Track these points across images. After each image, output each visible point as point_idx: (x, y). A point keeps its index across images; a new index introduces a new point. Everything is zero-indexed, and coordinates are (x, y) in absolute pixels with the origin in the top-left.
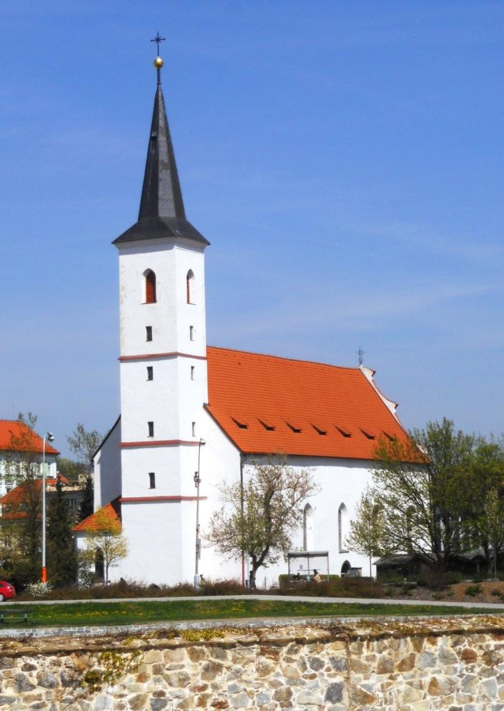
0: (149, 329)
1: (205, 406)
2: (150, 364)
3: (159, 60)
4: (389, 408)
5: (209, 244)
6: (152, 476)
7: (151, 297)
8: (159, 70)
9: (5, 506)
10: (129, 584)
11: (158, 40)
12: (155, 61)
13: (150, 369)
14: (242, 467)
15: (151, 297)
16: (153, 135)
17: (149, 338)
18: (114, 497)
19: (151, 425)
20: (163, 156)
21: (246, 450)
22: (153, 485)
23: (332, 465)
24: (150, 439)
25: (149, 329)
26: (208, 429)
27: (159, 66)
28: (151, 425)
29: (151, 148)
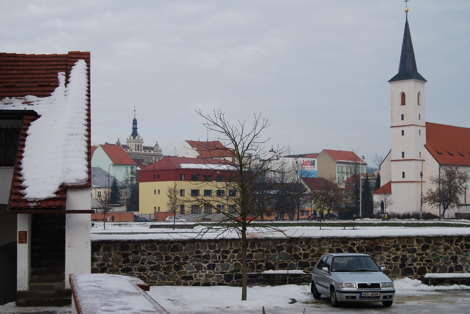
0: (402, 116)
3: (406, 10)
6: (403, 173)
8: (407, 13)
11: (406, 1)
19: (403, 153)
24: (403, 159)
25: (402, 116)
28: (403, 153)
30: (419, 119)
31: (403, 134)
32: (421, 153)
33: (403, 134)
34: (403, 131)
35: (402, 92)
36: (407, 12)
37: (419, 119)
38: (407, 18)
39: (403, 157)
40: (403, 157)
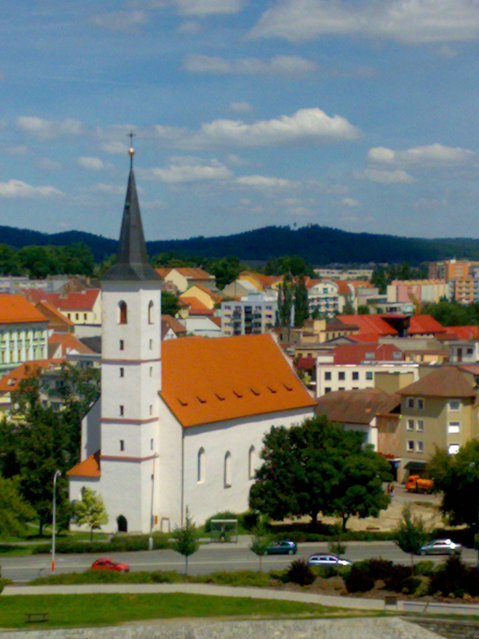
0: (122, 342)
1: (159, 393)
2: (122, 366)
3: (132, 150)
4: (164, 407)
6: (122, 442)
7: (124, 319)
8: (131, 159)
9: (201, 266)
10: (27, 289)
11: (131, 136)
12: (130, 151)
13: (122, 370)
14: (183, 437)
15: (124, 319)
16: (128, 205)
17: (122, 348)
18: (95, 451)
20: (133, 223)
21: (186, 424)
22: (122, 448)
23: (206, 431)
25: (122, 342)
26: (159, 408)
27: (131, 155)
28: (122, 408)
29: (67, 440)
38: (131, 167)
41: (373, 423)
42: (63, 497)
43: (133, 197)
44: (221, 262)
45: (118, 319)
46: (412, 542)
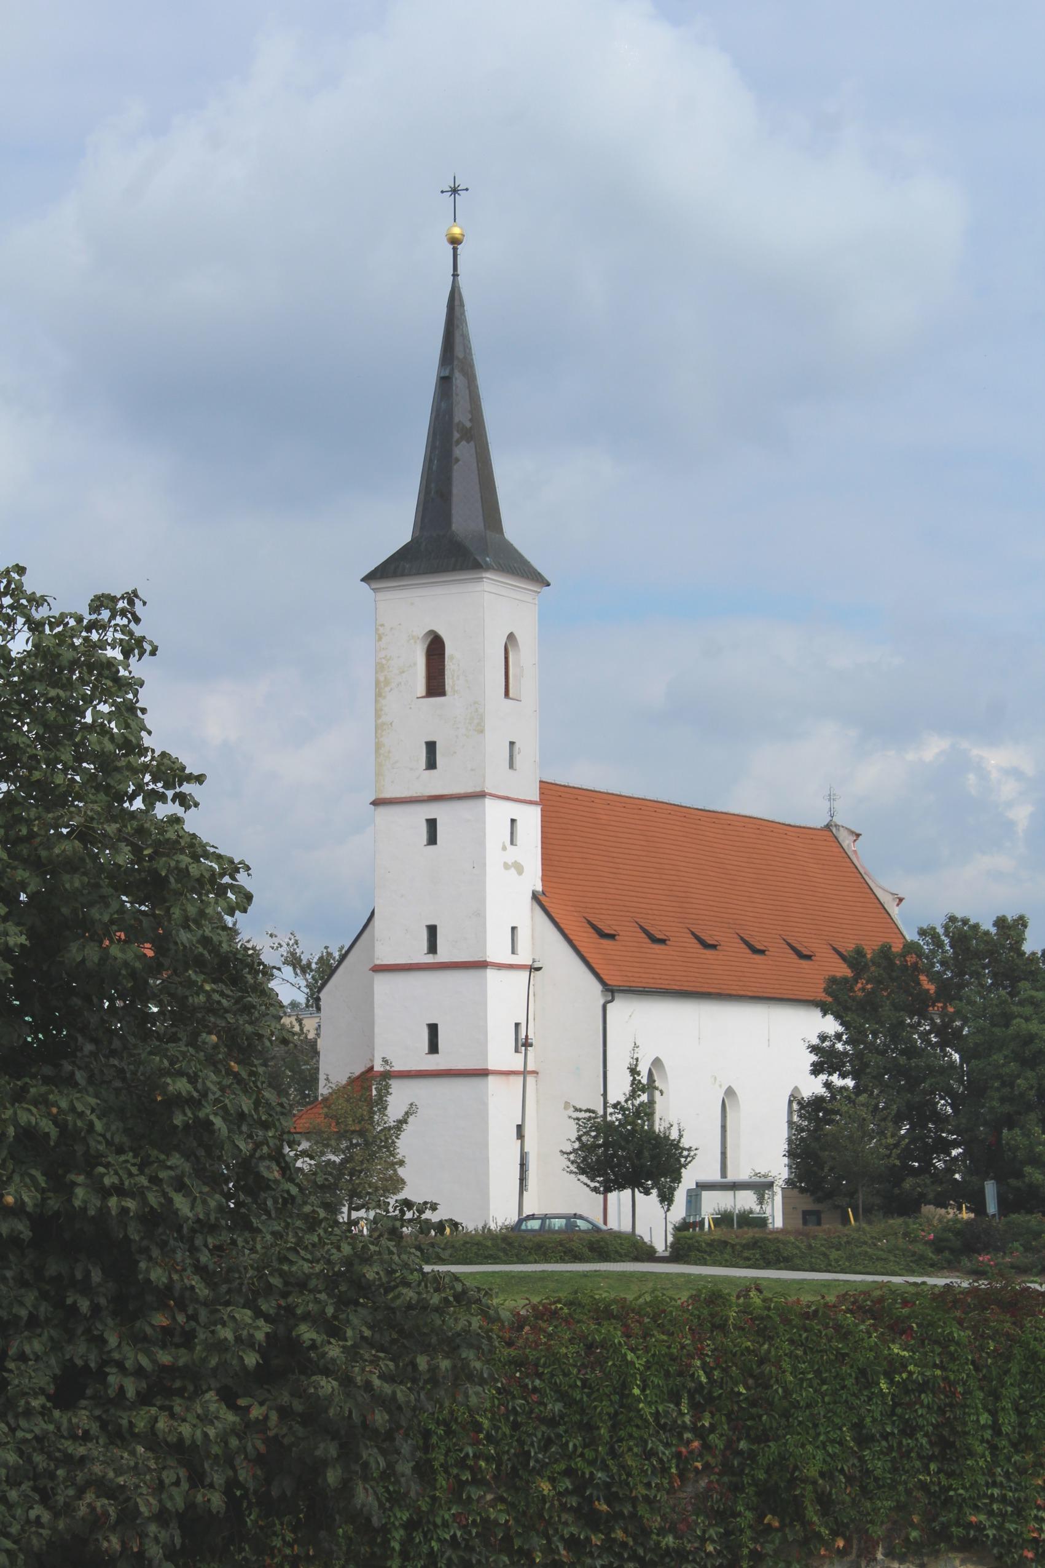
0: (431, 747)
1: (535, 897)
3: (456, 231)
5: (548, 585)
6: (433, 1029)
7: (435, 685)
8: (455, 250)
11: (455, 191)
15: (435, 685)
17: (431, 764)
19: (432, 930)
20: (461, 415)
22: (433, 1048)
24: (430, 959)
25: (431, 747)
28: (432, 930)
30: (511, 766)
31: (432, 840)
32: (519, 824)
33: (432, 840)
34: (432, 824)
35: (432, 632)
36: (455, 242)
37: (511, 766)
38: (455, 275)
39: (432, 948)
40: (432, 948)
41: (132, 1214)
42: (750, 1233)
43: (459, 352)
44: (314, 1336)
45: (421, 687)
46: (584, 1301)
